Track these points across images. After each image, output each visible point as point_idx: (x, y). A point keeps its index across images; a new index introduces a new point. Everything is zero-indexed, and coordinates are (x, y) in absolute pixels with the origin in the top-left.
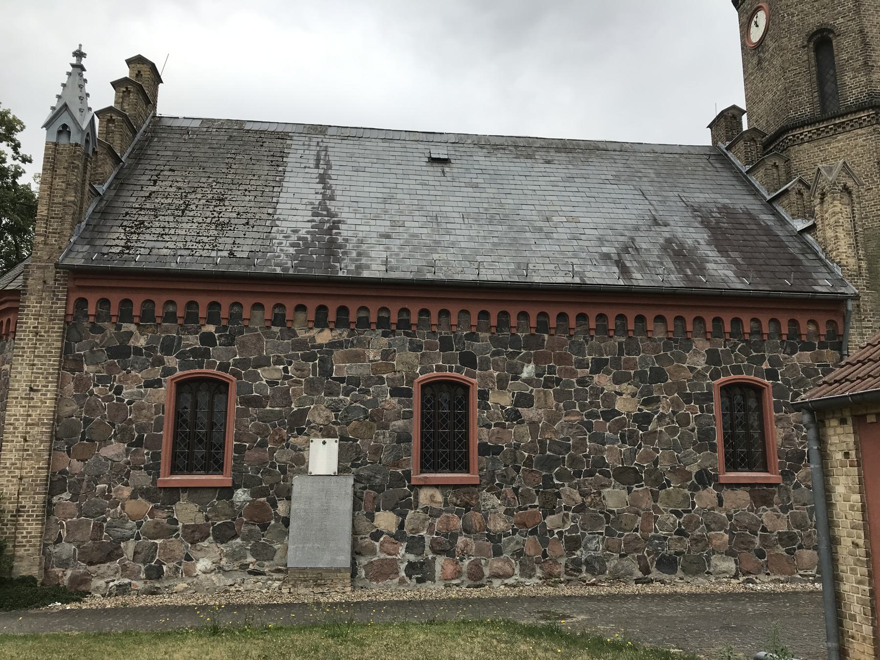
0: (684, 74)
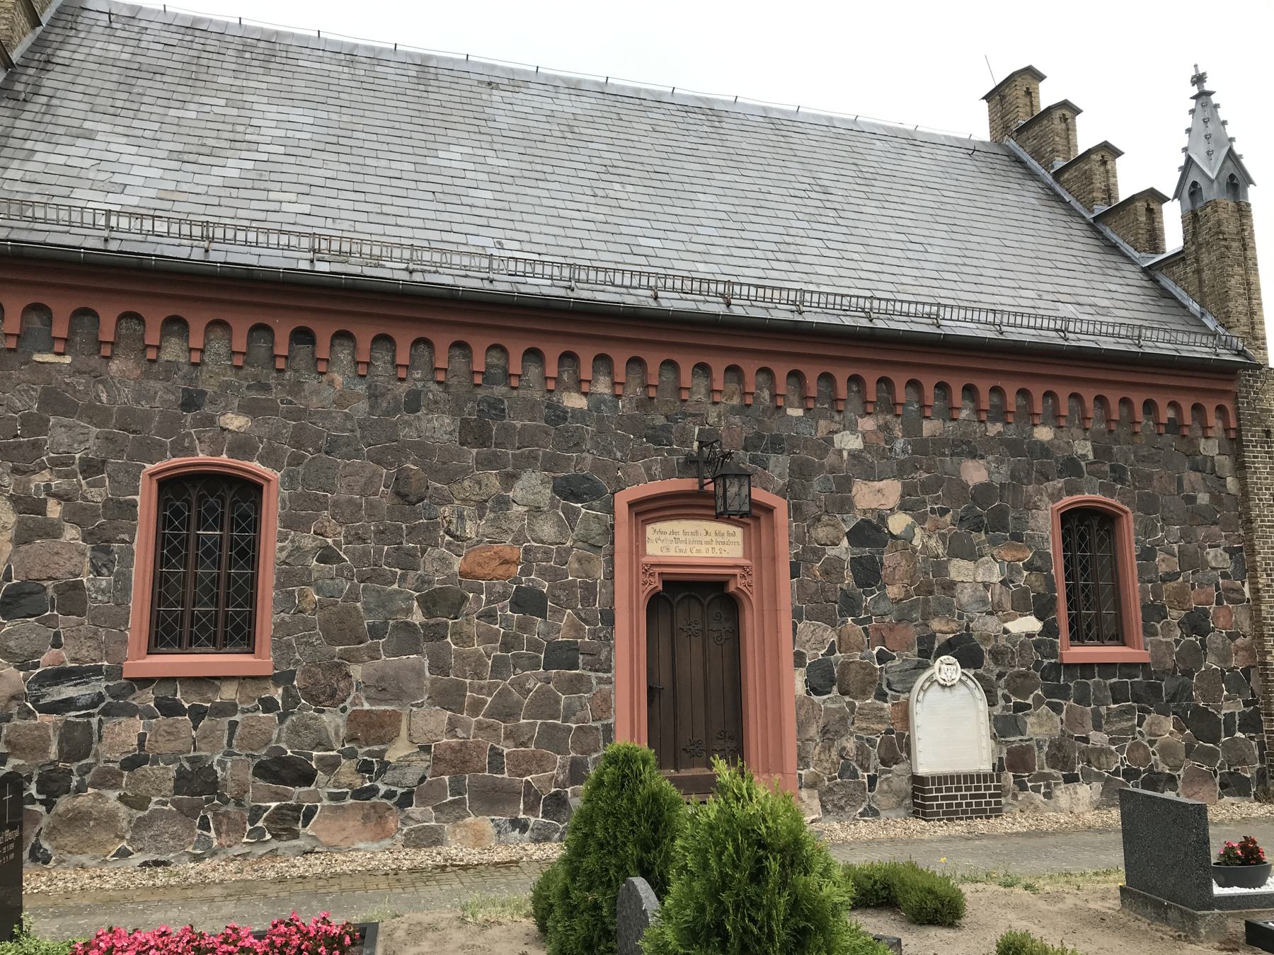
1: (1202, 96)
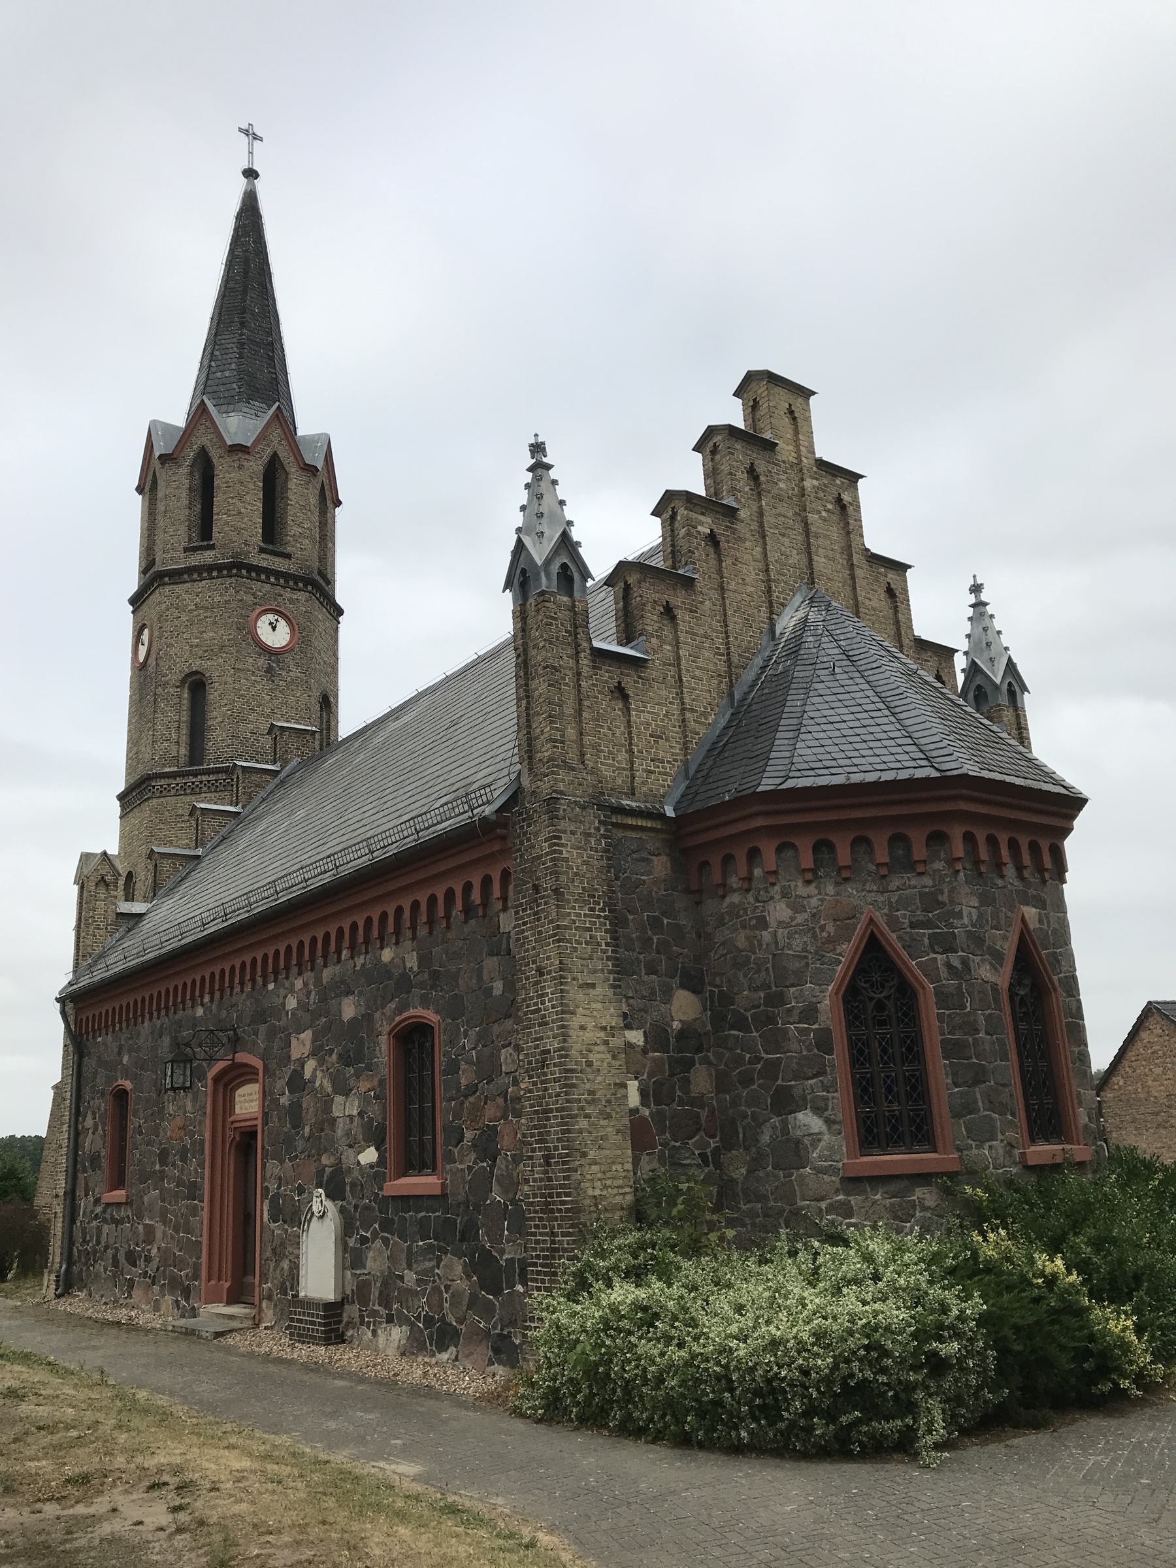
1: (979, 605)
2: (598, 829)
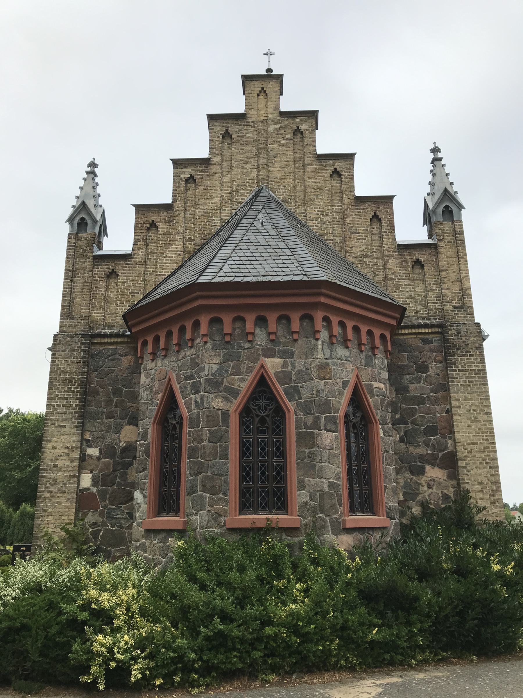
0: (513, 494)
2: (80, 347)
